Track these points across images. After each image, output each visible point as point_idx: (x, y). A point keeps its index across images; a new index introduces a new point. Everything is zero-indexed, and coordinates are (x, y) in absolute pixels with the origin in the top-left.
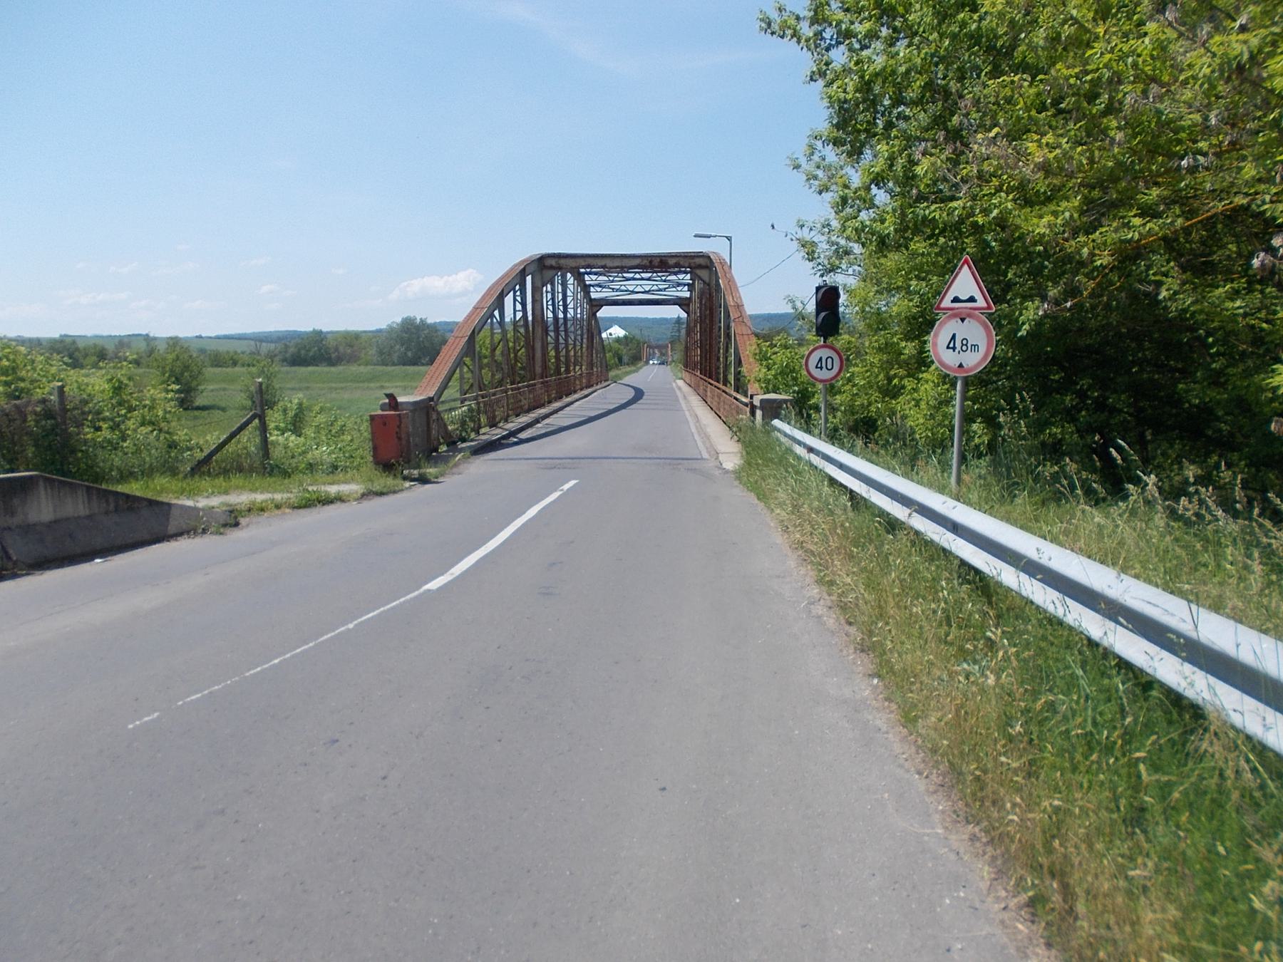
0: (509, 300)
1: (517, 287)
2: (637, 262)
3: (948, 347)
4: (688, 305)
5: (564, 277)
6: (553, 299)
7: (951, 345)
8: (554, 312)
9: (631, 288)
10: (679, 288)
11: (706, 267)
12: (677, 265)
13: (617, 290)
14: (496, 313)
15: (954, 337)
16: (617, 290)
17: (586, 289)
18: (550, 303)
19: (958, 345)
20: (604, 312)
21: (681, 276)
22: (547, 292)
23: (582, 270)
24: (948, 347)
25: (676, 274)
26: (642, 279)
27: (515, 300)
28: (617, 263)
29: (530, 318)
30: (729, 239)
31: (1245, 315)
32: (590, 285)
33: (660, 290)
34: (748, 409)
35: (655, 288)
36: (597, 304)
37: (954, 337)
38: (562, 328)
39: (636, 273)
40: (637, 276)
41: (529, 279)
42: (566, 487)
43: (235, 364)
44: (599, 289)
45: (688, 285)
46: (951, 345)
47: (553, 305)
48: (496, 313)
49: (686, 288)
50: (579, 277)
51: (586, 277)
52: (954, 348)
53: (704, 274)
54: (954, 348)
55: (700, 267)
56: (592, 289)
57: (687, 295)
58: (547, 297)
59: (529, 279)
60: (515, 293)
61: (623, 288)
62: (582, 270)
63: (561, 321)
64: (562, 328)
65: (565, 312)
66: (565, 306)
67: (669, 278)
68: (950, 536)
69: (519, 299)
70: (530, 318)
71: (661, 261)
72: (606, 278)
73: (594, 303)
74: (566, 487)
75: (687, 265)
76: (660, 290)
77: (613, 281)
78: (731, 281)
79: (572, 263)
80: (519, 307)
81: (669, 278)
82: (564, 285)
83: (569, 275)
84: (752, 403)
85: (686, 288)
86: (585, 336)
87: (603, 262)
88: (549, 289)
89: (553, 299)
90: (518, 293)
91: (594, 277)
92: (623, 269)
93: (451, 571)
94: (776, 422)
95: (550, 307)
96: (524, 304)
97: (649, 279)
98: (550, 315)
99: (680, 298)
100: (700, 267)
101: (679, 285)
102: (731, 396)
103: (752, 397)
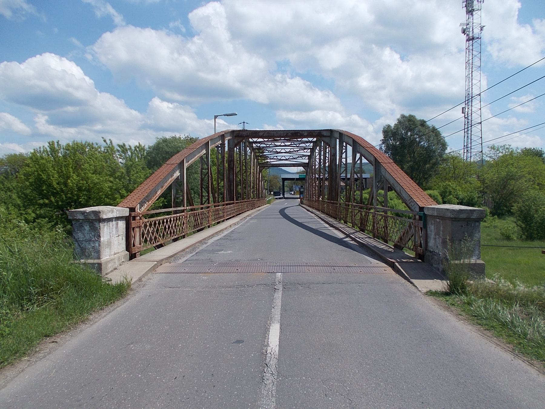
10: (305, 151)
26: (286, 146)
33: (294, 158)
35: (292, 150)
67: (301, 145)
76: (294, 158)
81: (301, 145)
101: (305, 149)
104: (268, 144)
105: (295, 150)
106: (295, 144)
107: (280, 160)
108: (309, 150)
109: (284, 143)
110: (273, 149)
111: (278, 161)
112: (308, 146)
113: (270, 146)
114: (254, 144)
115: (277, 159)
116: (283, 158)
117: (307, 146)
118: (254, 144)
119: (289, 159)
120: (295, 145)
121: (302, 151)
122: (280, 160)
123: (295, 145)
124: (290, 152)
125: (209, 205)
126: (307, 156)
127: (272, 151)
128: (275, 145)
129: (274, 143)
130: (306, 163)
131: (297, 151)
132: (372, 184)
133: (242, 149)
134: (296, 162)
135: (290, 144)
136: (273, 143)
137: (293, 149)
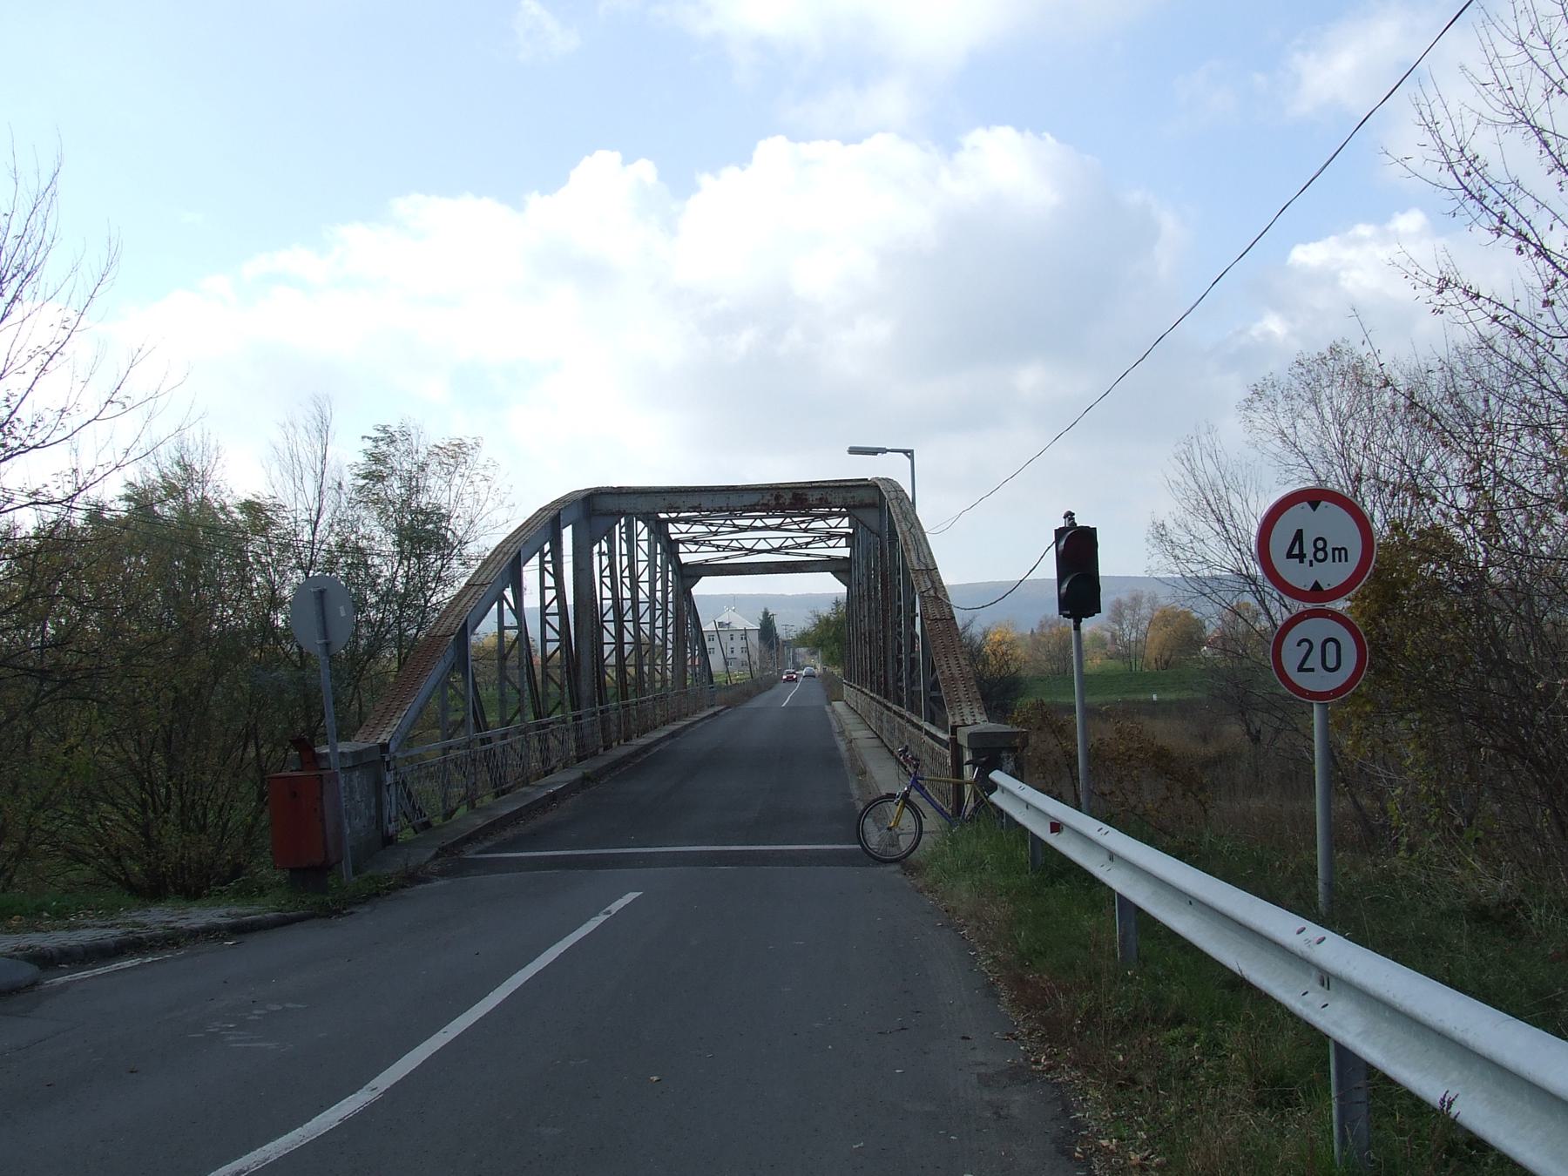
0: (530, 573)
1: (547, 547)
2: (754, 498)
3: (1290, 555)
4: (848, 571)
5: (630, 527)
6: (612, 565)
7: (1296, 551)
8: (613, 589)
9: (748, 544)
10: (831, 543)
11: (872, 506)
12: (823, 502)
13: (725, 548)
14: (508, 593)
15: (1299, 536)
16: (725, 548)
17: (671, 548)
18: (607, 573)
19: (1309, 549)
20: (704, 588)
21: (833, 522)
22: (601, 554)
23: (663, 516)
24: (1290, 555)
25: (824, 517)
26: (767, 528)
27: (543, 570)
28: (720, 501)
29: (570, 600)
30: (909, 453)
31: (1369, 689)
32: (678, 541)
33: (799, 546)
34: (948, 753)
35: (790, 542)
36: (691, 574)
37: (1299, 536)
38: (629, 616)
39: (755, 518)
40: (758, 523)
41: (567, 534)
42: (616, 906)
43: (852, 708)
44: (693, 548)
45: (847, 535)
46: (1296, 551)
47: (613, 576)
48: (508, 593)
49: (843, 542)
50: (659, 530)
51: (671, 528)
52: (1301, 557)
53: (871, 517)
54: (1301, 557)
55: (863, 506)
56: (682, 548)
57: (846, 553)
58: (598, 563)
59: (567, 534)
60: (543, 556)
61: (735, 544)
62: (663, 516)
63: (627, 604)
64: (629, 616)
65: (634, 588)
66: (635, 579)
67: (812, 525)
68: (1317, 996)
69: (549, 567)
70: (570, 600)
71: (795, 496)
72: (704, 529)
73: (685, 571)
74: (616, 906)
75: (839, 501)
76: (799, 546)
77: (716, 533)
78: (915, 524)
79: (644, 505)
80: (550, 581)
81: (812, 525)
82: (631, 541)
83: (640, 525)
84: (954, 741)
85: (843, 542)
86: (670, 630)
87: (695, 501)
88: (605, 547)
89: (612, 565)
90: (548, 558)
91: (684, 527)
92: (733, 512)
93: (373, 1083)
94: (996, 776)
95: (607, 581)
96: (558, 576)
97: (778, 528)
98: (607, 594)
99: (831, 560)
100: (863, 506)
101: (830, 536)
102: (920, 728)
103: (954, 729)
104: (711, 525)
105: (798, 541)
106: (795, 523)
107: (751, 551)
108: (844, 539)
109: (761, 519)
110: (732, 540)
111: (746, 555)
112: (836, 527)
113: (721, 529)
114: (670, 525)
115: (740, 549)
116: (762, 545)
117: (831, 528)
118: (670, 525)
119: (780, 547)
120: (796, 527)
121: (823, 545)
122: (751, 551)
123: (796, 527)
124: (786, 547)
125: (581, 712)
126: (842, 536)
127: (726, 547)
128: (734, 526)
129: (731, 520)
130: (845, 558)
131: (808, 543)
132: (701, 709)
133: (621, 533)
134: (808, 555)
135: (779, 521)
136: (729, 522)
137: (792, 538)
